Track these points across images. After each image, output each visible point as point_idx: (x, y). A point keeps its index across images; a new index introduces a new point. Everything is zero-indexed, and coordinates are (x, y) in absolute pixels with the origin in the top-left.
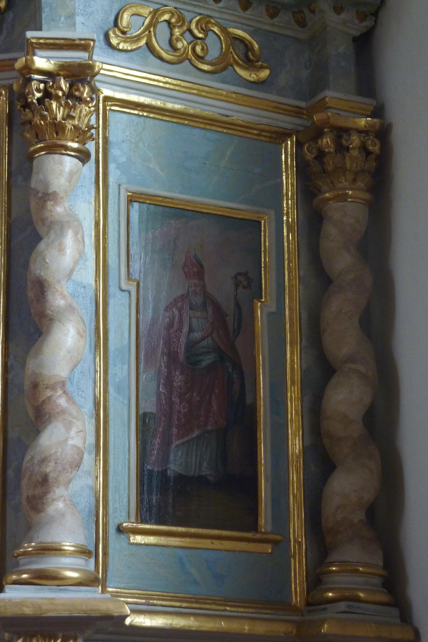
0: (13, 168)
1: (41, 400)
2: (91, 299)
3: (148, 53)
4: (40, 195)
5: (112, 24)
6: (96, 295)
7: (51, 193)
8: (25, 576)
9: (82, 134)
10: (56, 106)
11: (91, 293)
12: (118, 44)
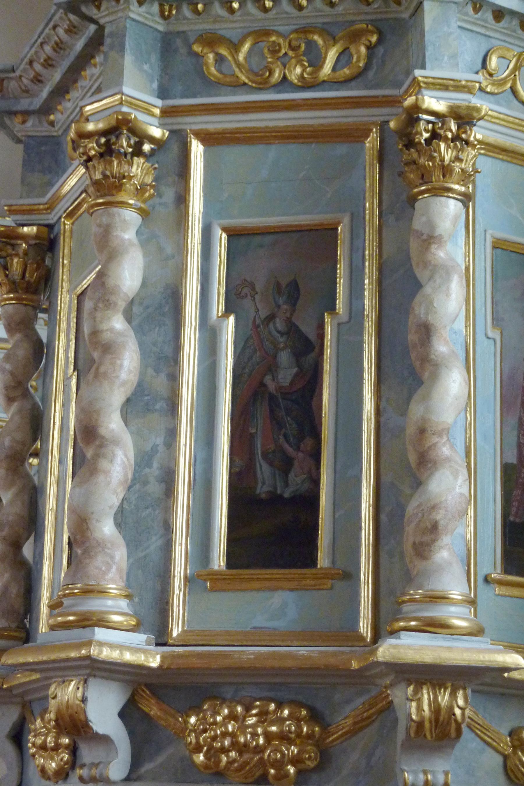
0: (384, 207)
1: (426, 446)
2: (461, 345)
3: (512, 97)
4: (424, 237)
5: (480, 65)
6: (466, 342)
7: (437, 237)
8: (413, 623)
9: (466, 177)
10: (445, 147)
11: (462, 340)
12: (487, 86)
